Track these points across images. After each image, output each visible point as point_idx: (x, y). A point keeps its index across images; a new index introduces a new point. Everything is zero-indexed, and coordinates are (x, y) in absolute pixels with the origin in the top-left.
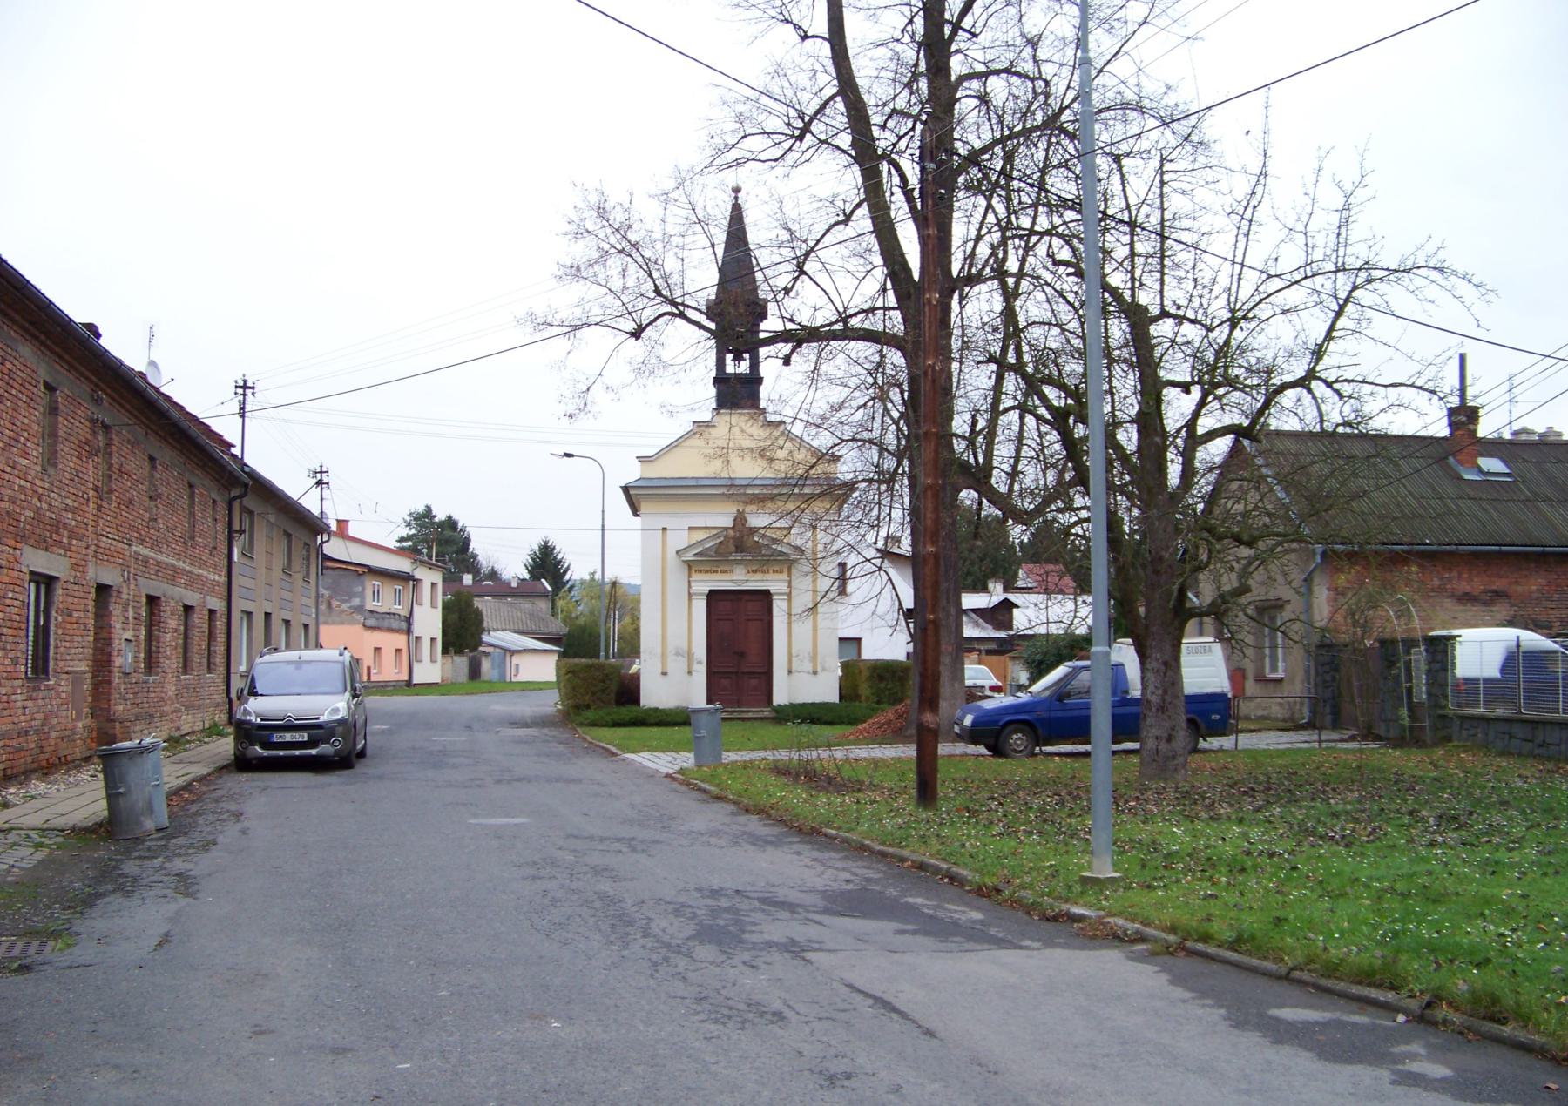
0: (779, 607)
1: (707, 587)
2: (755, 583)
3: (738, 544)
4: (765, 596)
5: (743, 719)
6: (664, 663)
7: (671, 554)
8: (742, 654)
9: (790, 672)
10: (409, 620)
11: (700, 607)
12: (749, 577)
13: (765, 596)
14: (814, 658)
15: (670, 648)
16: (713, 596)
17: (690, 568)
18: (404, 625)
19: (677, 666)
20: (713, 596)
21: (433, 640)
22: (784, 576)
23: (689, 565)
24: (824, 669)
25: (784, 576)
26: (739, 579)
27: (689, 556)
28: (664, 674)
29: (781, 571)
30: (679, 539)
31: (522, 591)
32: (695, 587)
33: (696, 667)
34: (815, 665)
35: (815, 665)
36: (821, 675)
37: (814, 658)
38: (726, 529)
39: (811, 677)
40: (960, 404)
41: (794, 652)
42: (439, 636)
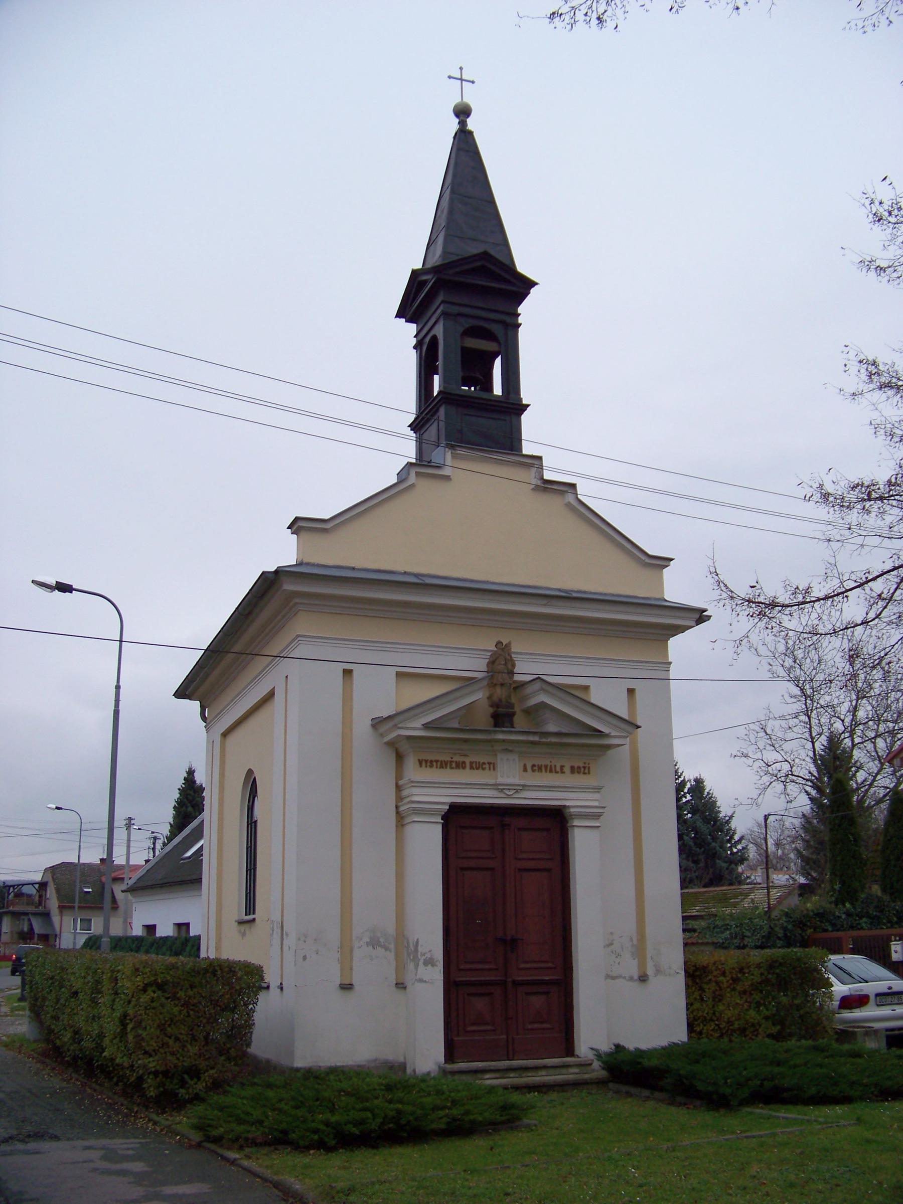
0: (583, 845)
1: (444, 798)
2: (538, 793)
3: (504, 712)
4: (554, 822)
7: (362, 727)
8: (511, 944)
11: (427, 843)
13: (554, 822)
16: (458, 819)
17: (400, 758)
20: (458, 819)
23: (398, 752)
24: (658, 971)
26: (508, 782)
28: (347, 987)
30: (379, 694)
31: (22, 973)
34: (642, 964)
35: (642, 964)
36: (654, 982)
38: (469, 682)
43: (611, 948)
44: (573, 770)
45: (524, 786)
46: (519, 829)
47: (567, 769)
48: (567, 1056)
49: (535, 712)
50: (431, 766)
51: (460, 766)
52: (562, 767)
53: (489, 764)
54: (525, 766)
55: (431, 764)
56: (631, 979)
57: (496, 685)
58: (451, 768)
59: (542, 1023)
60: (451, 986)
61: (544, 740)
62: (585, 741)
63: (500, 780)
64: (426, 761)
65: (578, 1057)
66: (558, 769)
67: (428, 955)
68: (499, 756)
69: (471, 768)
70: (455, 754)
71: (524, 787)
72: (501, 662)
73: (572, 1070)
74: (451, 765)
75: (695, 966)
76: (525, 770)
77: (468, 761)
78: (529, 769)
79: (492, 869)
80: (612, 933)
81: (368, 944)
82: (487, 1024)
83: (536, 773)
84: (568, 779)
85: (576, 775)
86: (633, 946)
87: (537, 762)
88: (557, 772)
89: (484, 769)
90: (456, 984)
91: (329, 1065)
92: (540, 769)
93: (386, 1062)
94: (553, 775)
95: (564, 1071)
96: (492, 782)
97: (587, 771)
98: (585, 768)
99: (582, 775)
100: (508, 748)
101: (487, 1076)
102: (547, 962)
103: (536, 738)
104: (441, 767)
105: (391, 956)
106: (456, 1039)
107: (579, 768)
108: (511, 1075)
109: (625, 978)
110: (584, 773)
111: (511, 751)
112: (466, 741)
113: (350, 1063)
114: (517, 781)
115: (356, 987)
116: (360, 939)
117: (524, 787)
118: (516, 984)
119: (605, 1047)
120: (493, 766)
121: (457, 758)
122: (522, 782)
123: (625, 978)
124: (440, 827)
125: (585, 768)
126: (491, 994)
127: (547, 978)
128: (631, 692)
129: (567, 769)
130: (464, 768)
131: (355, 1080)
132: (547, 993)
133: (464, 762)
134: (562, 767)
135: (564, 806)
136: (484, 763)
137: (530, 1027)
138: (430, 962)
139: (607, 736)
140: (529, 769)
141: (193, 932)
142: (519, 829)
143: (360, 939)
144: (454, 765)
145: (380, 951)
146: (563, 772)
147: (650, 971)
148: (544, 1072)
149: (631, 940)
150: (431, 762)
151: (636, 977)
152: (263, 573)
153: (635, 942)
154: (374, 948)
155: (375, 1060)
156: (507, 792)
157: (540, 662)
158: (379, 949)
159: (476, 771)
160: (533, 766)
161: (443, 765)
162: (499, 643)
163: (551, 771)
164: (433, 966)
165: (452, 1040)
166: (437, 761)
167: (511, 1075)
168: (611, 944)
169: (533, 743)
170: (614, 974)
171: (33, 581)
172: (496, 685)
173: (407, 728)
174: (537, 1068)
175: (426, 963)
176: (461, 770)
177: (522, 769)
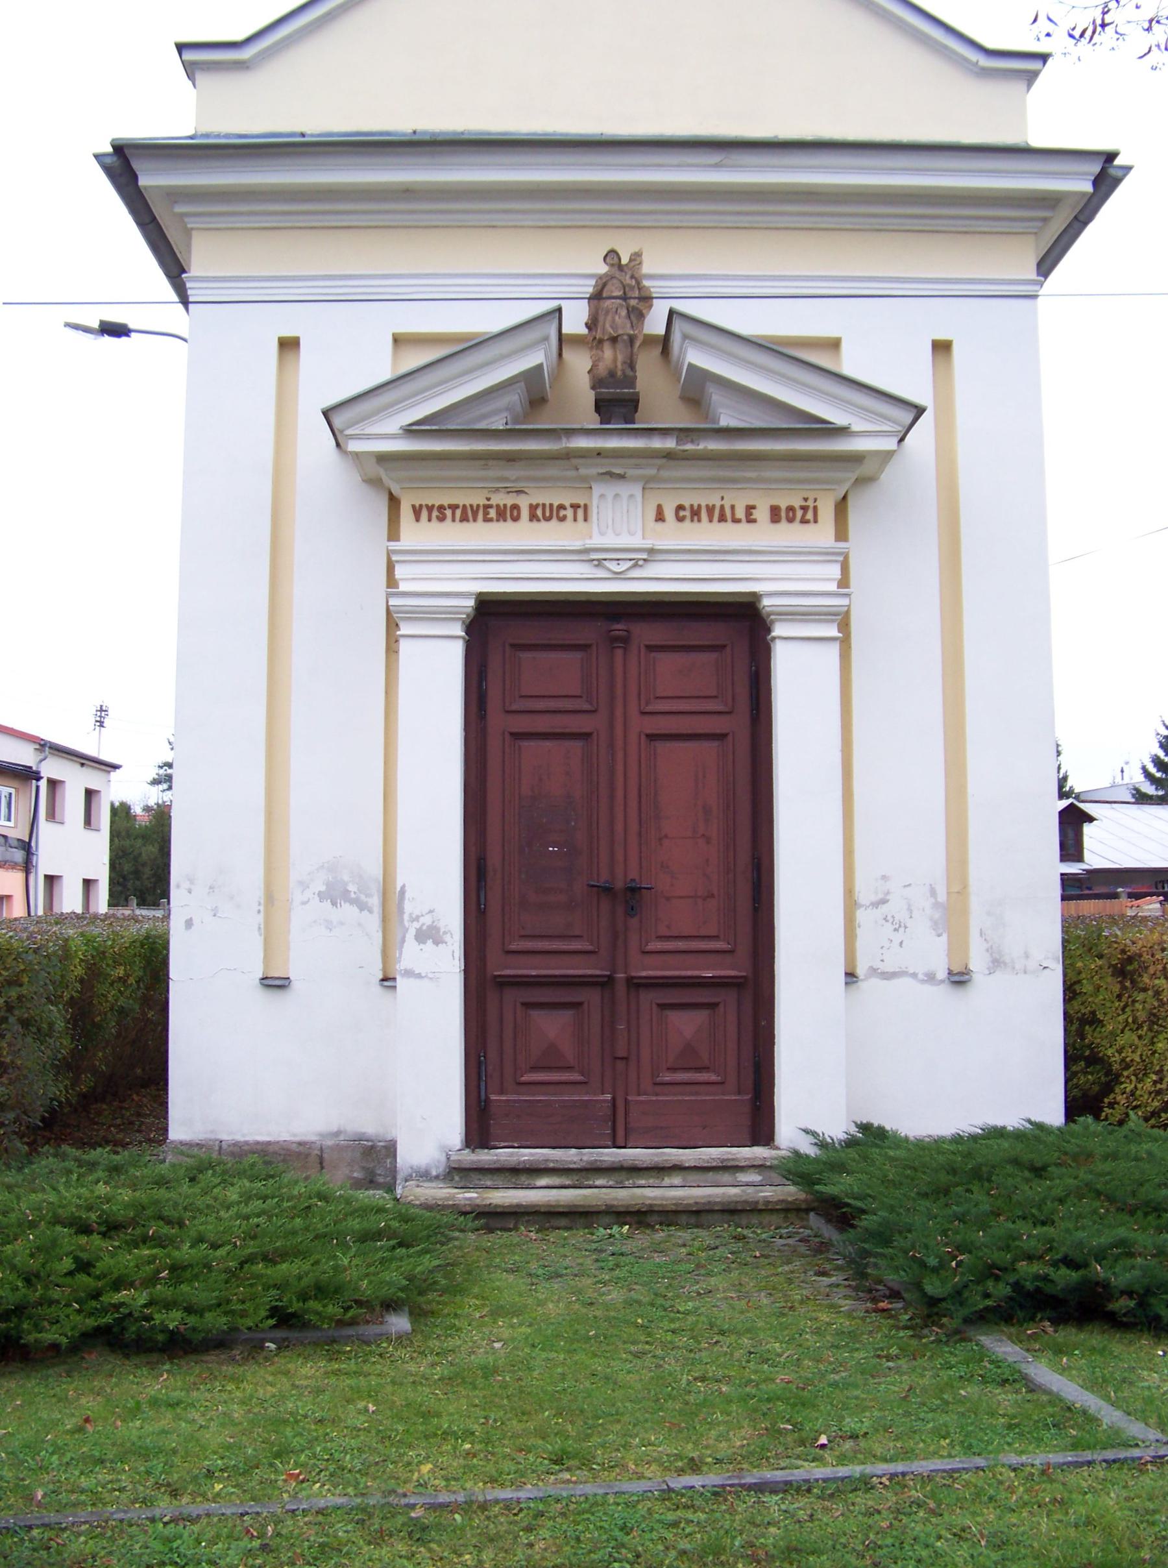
0: (799, 676)
2: (689, 561)
3: (621, 392)
4: (737, 629)
5: (640, 1217)
6: (272, 937)
8: (631, 898)
9: (851, 976)
10: (27, 847)
11: (437, 671)
12: (673, 536)
13: (737, 629)
14: (953, 914)
15: (307, 856)
16: (498, 627)
18: (19, 856)
19: (330, 949)
20: (498, 627)
21: (88, 883)
22: (822, 534)
24: (997, 963)
25: (822, 534)
26: (620, 542)
27: (385, 434)
28: (275, 984)
29: (805, 515)
30: (352, 351)
32: (409, 577)
33: (412, 955)
34: (958, 942)
35: (958, 942)
37: (953, 914)
39: (942, 993)
40: (453, 1197)
41: (865, 892)
42: (102, 874)
43: (884, 909)
44: (775, 515)
45: (651, 551)
46: (651, 648)
47: (762, 514)
48: (755, 1142)
49: (696, 389)
50: (442, 519)
51: (507, 514)
52: (750, 509)
53: (575, 507)
54: (660, 509)
55: (440, 513)
56: (930, 978)
57: (601, 341)
58: (487, 520)
59: (699, 1069)
60: (484, 989)
61: (689, 447)
62: (804, 454)
63: (597, 541)
64: (430, 509)
65: (778, 1148)
66: (740, 513)
67: (427, 920)
68: (598, 489)
69: (533, 517)
70: (497, 490)
71: (652, 554)
72: (620, 293)
73: (743, 1177)
74: (486, 514)
75: (1123, 952)
76: (660, 517)
77: (524, 503)
78: (669, 513)
79: (585, 736)
80: (884, 878)
81: (321, 896)
82: (569, 1068)
83: (687, 523)
84: (765, 535)
85: (784, 525)
86: (936, 905)
87: (689, 499)
88: (736, 521)
89: (562, 519)
90: (504, 983)
91: (239, 1138)
92: (695, 513)
93: (360, 1138)
94: (729, 526)
95: (726, 1178)
96: (577, 545)
97: (810, 516)
98: (805, 509)
99: (796, 526)
100: (614, 469)
101: (543, 1181)
102: (716, 938)
103: (670, 444)
104: (464, 519)
105: (373, 922)
106: (493, 1097)
107: (791, 509)
108: (598, 1182)
109: (914, 975)
110: (804, 521)
111: (622, 477)
112: (510, 458)
113: (285, 1136)
114: (636, 541)
115: (295, 984)
116: (303, 885)
117: (652, 554)
118: (636, 985)
119: (837, 1129)
120: (582, 511)
121: (499, 499)
122: (648, 543)
123: (914, 975)
124: (456, 651)
125: (805, 509)
126: (577, 1005)
127: (534, 973)
128: (942, 348)
129: (762, 514)
130: (516, 519)
131: (185, 1188)
132: (713, 1006)
133: (515, 507)
134: (750, 509)
135: (754, 594)
136: (561, 507)
137: (668, 1077)
138: (430, 935)
139: (842, 431)
140: (669, 513)
141: (323, 888)
142: (651, 648)
143: (303, 885)
144: (493, 513)
145: (349, 911)
146: (751, 521)
147: (977, 963)
148: (677, 1180)
149: (933, 893)
150: (441, 508)
151: (942, 974)
152: (586, 324)
153: (942, 897)
154: (334, 904)
155: (337, 1133)
156: (613, 566)
157: (733, 294)
158: (346, 906)
159: (544, 525)
160: (680, 508)
161: (467, 514)
162: (611, 255)
163: (722, 519)
164: (437, 943)
165: (487, 1100)
166: (454, 507)
167: (598, 1182)
168: (884, 901)
169: (669, 455)
170: (888, 967)
171: (67, 325)
172: (601, 341)
173: (369, 437)
174: (661, 1170)
175: (421, 937)
176: (510, 523)
177: (652, 514)
